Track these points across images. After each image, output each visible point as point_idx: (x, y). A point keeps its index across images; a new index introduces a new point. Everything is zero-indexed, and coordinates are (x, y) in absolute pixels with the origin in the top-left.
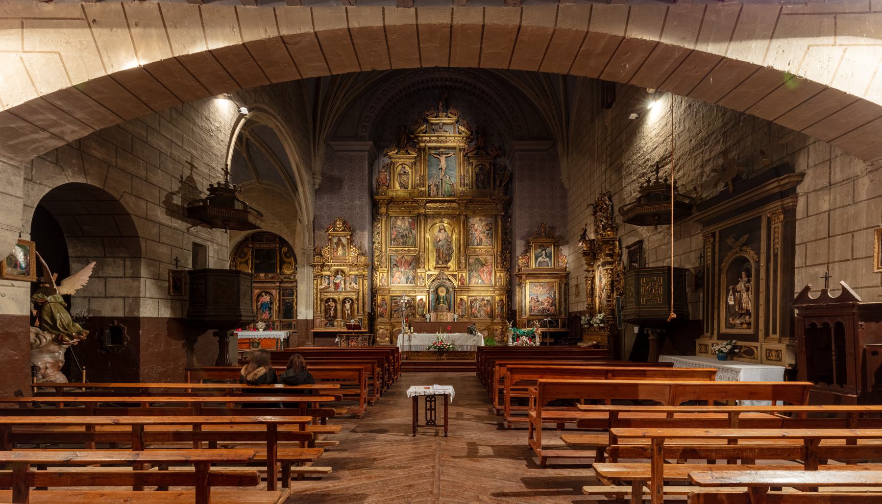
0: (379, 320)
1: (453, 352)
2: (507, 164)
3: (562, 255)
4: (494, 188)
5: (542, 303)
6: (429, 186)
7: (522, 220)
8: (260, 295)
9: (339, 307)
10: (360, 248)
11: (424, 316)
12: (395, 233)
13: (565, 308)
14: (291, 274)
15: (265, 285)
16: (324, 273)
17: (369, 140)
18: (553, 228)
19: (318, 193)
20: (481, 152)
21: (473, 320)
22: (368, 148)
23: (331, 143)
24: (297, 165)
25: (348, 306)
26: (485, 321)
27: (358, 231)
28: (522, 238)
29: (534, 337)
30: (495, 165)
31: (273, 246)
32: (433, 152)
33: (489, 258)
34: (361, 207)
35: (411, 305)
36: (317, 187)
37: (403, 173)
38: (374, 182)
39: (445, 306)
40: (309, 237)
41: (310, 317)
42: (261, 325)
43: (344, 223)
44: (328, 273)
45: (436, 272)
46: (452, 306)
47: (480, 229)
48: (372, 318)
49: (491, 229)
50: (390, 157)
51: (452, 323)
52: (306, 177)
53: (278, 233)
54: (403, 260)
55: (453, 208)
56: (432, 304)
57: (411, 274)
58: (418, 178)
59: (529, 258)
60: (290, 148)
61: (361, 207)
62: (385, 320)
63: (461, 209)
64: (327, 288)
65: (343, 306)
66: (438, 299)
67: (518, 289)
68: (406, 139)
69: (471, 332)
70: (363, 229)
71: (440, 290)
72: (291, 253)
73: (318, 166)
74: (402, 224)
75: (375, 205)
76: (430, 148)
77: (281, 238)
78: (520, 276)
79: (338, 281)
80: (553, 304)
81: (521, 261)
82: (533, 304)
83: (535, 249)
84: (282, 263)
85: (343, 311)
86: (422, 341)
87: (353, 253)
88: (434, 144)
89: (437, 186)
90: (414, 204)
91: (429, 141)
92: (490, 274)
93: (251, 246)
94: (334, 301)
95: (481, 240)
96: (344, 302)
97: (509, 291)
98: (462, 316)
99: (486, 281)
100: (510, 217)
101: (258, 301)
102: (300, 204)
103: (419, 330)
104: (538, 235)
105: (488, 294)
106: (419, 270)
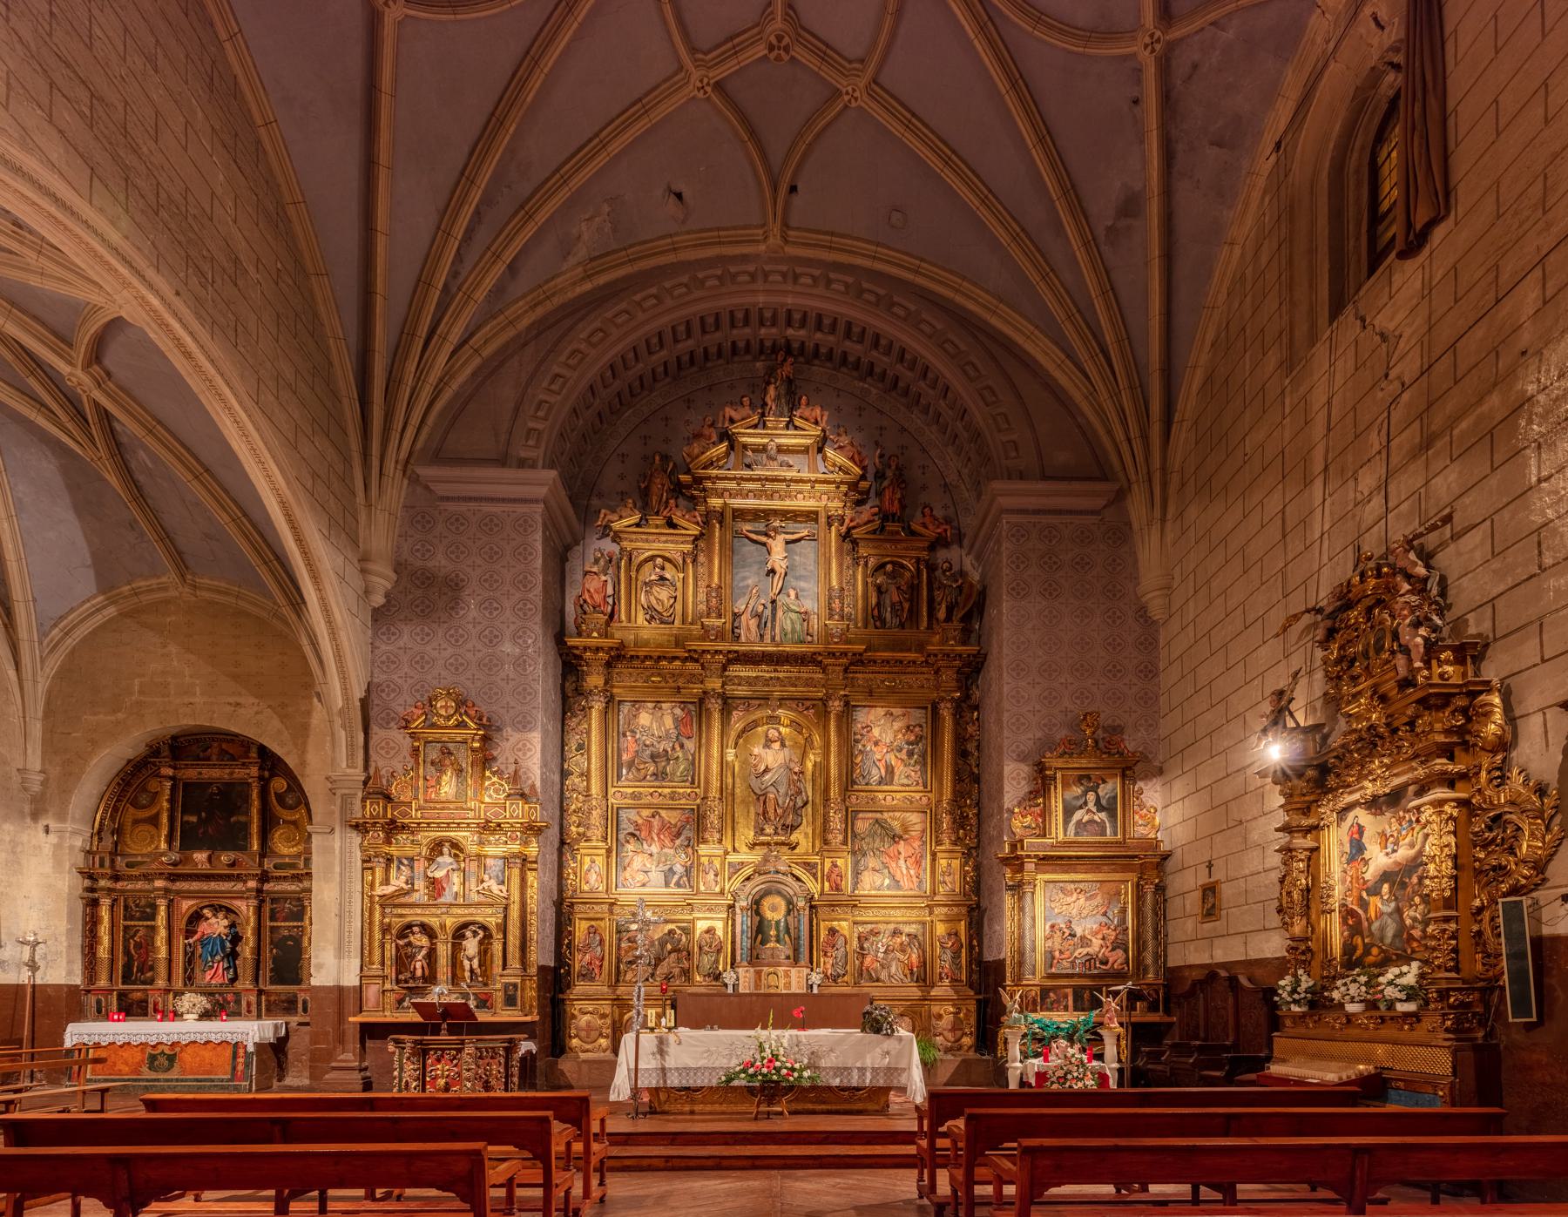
0: (580, 988)
1: (814, 1088)
2: (968, 566)
3: (1142, 806)
4: (930, 626)
5: (1085, 941)
6: (736, 616)
7: (1019, 707)
8: (196, 917)
9: (444, 951)
10: (515, 778)
11: (717, 977)
12: (633, 747)
13: (1156, 956)
14: (298, 856)
15: (213, 885)
16: (393, 850)
17: (552, 466)
18: (1117, 730)
19: (381, 617)
20: (891, 526)
21: (868, 989)
22: (542, 491)
23: (425, 472)
24: (283, 504)
25: (471, 946)
26: (903, 992)
27: (508, 731)
28: (1022, 758)
29: (1099, 1040)
30: (932, 568)
31: (240, 773)
32: (747, 527)
33: (914, 818)
34: (520, 663)
35: (677, 950)
36: (378, 600)
37: (654, 580)
38: (570, 608)
39: (784, 950)
40: (351, 746)
41: (351, 979)
42: (191, 1001)
43: (461, 703)
44: (410, 851)
45: (754, 857)
46: (804, 950)
47: (888, 738)
48: (555, 983)
49: (919, 739)
50: (617, 538)
51: (807, 998)
52: (328, 556)
53: (249, 732)
54: (656, 822)
55: (809, 683)
56: (743, 942)
57: (679, 862)
58: (702, 597)
59: (1045, 814)
60: (232, 414)
61: (520, 663)
62: (600, 987)
63: (827, 679)
64: (402, 893)
65: (457, 948)
66: (760, 930)
67: (1008, 901)
68: (670, 487)
69: (874, 1025)
70: (524, 725)
71: (767, 903)
72: (297, 796)
73: (380, 535)
74: (653, 723)
75: (570, 666)
76: (739, 514)
77: (263, 751)
78: (1015, 862)
79: (439, 874)
80: (1119, 945)
81: (1020, 823)
82: (1057, 942)
83: (1066, 785)
84: (268, 823)
85: (455, 963)
86: (706, 1053)
87: (491, 796)
88: (751, 503)
89: (759, 616)
90: (690, 665)
91: (733, 491)
92: (918, 863)
93: (170, 772)
94: (426, 929)
95: (890, 770)
96: (459, 934)
97: (975, 910)
99: (905, 883)
100: (977, 708)
101: (189, 933)
102: (314, 644)
104: (1072, 747)
105: (913, 915)
106: (703, 850)
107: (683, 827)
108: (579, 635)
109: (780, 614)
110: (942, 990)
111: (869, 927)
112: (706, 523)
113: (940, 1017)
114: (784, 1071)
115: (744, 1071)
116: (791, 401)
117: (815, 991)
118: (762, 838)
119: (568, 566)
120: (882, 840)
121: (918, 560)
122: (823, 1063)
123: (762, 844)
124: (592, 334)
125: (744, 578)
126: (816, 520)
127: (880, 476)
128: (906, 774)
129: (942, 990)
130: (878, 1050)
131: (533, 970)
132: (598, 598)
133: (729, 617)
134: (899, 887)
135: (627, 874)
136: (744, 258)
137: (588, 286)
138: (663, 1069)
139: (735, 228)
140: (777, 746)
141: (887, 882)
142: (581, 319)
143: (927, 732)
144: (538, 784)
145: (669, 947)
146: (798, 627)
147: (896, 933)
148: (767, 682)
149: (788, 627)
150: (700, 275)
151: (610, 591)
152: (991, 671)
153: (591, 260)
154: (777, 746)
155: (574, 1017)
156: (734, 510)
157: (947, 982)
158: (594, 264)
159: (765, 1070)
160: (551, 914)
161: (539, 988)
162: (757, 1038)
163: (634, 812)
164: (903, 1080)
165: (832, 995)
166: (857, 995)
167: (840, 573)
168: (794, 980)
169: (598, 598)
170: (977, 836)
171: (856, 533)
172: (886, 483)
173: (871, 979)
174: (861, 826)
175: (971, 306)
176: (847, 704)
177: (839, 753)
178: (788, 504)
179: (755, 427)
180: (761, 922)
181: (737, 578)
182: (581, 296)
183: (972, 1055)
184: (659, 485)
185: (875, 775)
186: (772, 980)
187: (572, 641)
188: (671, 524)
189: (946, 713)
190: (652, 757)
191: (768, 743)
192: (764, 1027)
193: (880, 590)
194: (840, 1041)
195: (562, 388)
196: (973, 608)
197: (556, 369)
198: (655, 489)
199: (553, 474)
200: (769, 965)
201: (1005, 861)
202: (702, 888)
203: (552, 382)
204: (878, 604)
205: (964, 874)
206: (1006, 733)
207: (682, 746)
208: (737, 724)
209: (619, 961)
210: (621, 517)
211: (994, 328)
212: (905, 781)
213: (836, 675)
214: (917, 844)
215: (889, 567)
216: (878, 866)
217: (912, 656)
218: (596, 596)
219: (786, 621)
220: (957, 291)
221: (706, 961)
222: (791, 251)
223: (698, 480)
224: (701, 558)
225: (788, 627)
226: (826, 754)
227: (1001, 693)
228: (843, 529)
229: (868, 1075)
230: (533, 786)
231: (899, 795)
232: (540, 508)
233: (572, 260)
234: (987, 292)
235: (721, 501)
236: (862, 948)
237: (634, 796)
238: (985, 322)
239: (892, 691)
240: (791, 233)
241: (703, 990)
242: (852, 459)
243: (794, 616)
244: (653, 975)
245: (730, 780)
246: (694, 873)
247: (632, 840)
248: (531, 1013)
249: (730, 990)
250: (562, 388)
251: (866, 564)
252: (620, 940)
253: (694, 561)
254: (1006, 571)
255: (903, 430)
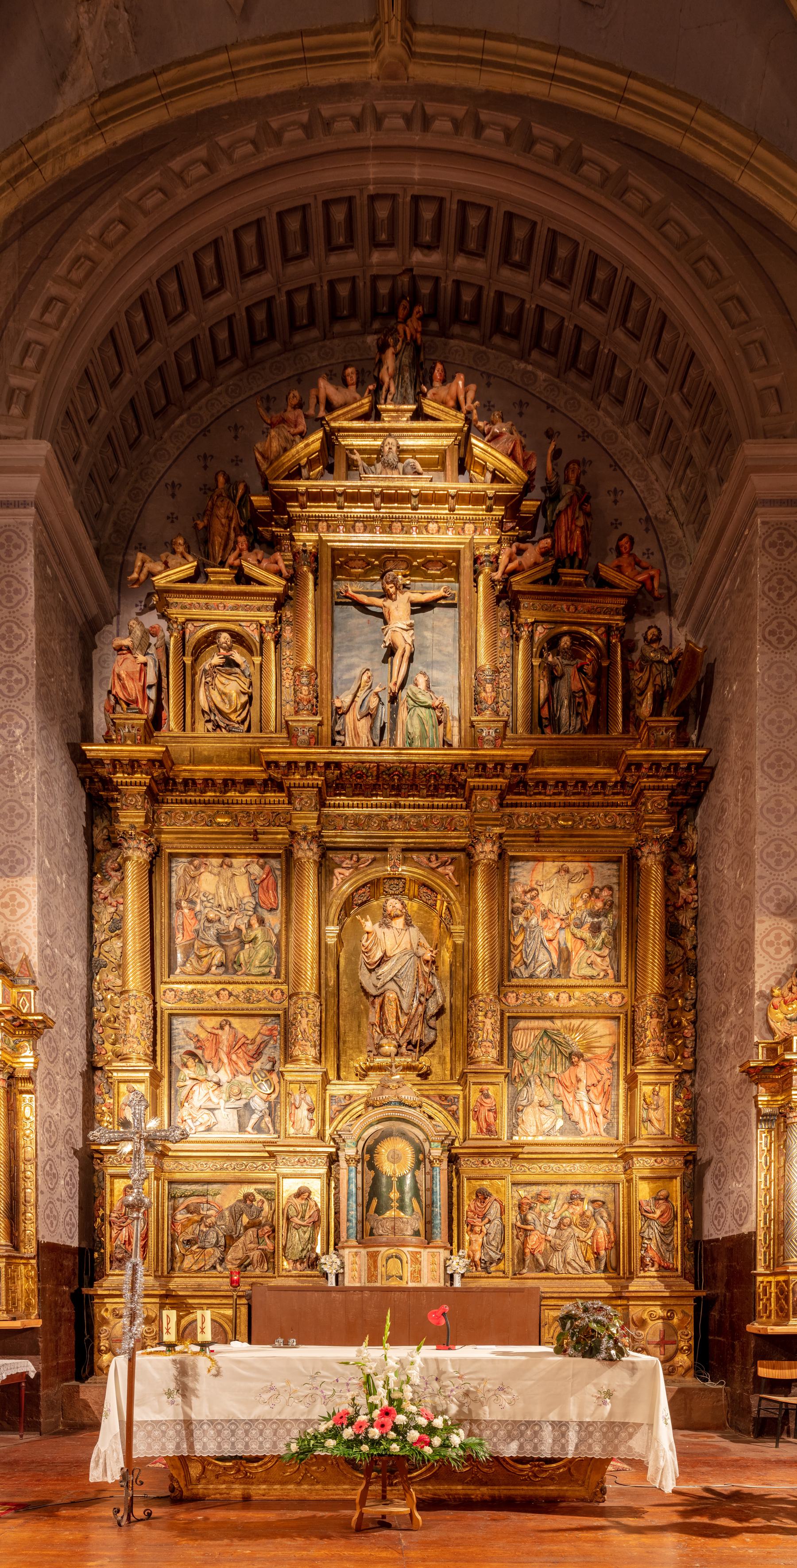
6: (339, 713)
11: (314, 1263)
12: (192, 925)
20: (570, 574)
21: (532, 1280)
28: (781, 911)
35: (258, 1222)
37: (217, 658)
39: (411, 1221)
46: (441, 1221)
47: (561, 906)
49: (609, 906)
54: (225, 1036)
56: (350, 1210)
63: (472, 807)
66: (374, 1193)
71: (384, 1151)
74: (220, 888)
75: (97, 795)
88: (361, 539)
89: (371, 715)
97: (694, 1161)
98: (486, 1265)
99: (587, 1125)
100: (693, 859)
103: (255, 1323)
107: (265, 1044)
108: (108, 741)
109: (403, 714)
110: (646, 1282)
111: (535, 1189)
112: (293, 579)
113: (642, 1324)
114: (413, 1435)
115: (335, 1433)
116: (419, 377)
117: (457, 1283)
118: (379, 1060)
119: (96, 655)
120: (554, 1062)
121: (609, 628)
122: (486, 1413)
123: (380, 1068)
124: (106, 228)
125: (351, 667)
126: (456, 572)
127: (552, 495)
128: (590, 960)
129: (646, 1282)
130: (591, 1389)
131: (29, 1250)
132: (133, 688)
133: (327, 714)
134: (579, 1132)
135: (184, 1113)
136: (344, 90)
137: (98, 146)
138: (188, 1423)
139: (329, 30)
140: (399, 923)
141: (560, 1123)
142: (90, 202)
143: (619, 896)
144: (34, 959)
145: (245, 1220)
146: (431, 733)
147: (573, 1198)
148: (384, 823)
149: (416, 730)
150: (275, 125)
151: (151, 678)
152: (726, 788)
153: (103, 95)
154: (399, 923)
155: (105, 1321)
156: (336, 553)
157: (652, 1271)
158: (107, 102)
159: (375, 1433)
160: (68, 1170)
161: (41, 1277)
162: (360, 1365)
163: (194, 1020)
164: (636, 1445)
165: (484, 1290)
166: (520, 1290)
167: (493, 644)
168: (424, 1267)
169: (133, 688)
170: (694, 1053)
171: (518, 583)
172: (561, 505)
173: (537, 1266)
174: (525, 1038)
175: (709, 157)
176: (501, 855)
177: (490, 927)
178: (415, 539)
179: (365, 417)
180: (376, 1180)
181: (339, 666)
182: (88, 165)
183: (691, 1381)
184: (224, 515)
185: (545, 961)
186: (393, 1267)
187: (95, 750)
188: (242, 578)
189: (651, 861)
190: (220, 938)
191: (387, 918)
192: (376, 1341)
193: (553, 679)
194: (519, 1372)
195: (60, 319)
196: (693, 693)
197: (52, 289)
198: (218, 526)
199: (43, 448)
200: (388, 1245)
201: (756, 1075)
202: (291, 1131)
203: (46, 309)
204: (549, 699)
205: (676, 1110)
206: (759, 869)
207: (261, 922)
208: (344, 881)
209: (174, 1240)
210: (167, 566)
211: (743, 195)
212: (588, 972)
213: (486, 802)
214: (604, 1066)
215: (565, 641)
216: (548, 1099)
217: (600, 772)
218: (129, 685)
219: (411, 721)
220: (687, 129)
221: (297, 1239)
222: (419, 72)
223: (281, 501)
224: (288, 634)
225: (416, 730)
226: (470, 934)
227: (748, 811)
228: (498, 576)
229: (572, 1437)
230: (25, 961)
231: (577, 993)
232: (29, 515)
233: (71, 94)
234: (736, 126)
235: (314, 536)
236: (525, 1221)
237: (193, 996)
238: (732, 186)
239: (569, 834)
240: (419, 36)
241: (291, 1282)
242: (512, 456)
243: (425, 713)
244: (222, 1261)
245: (332, 974)
246: (281, 1110)
247: (191, 1062)
248: (28, 1316)
249: (332, 1282)
250: (60, 319)
251: (531, 637)
252: (175, 1209)
253: (278, 640)
254: (761, 603)
255: (585, 434)
